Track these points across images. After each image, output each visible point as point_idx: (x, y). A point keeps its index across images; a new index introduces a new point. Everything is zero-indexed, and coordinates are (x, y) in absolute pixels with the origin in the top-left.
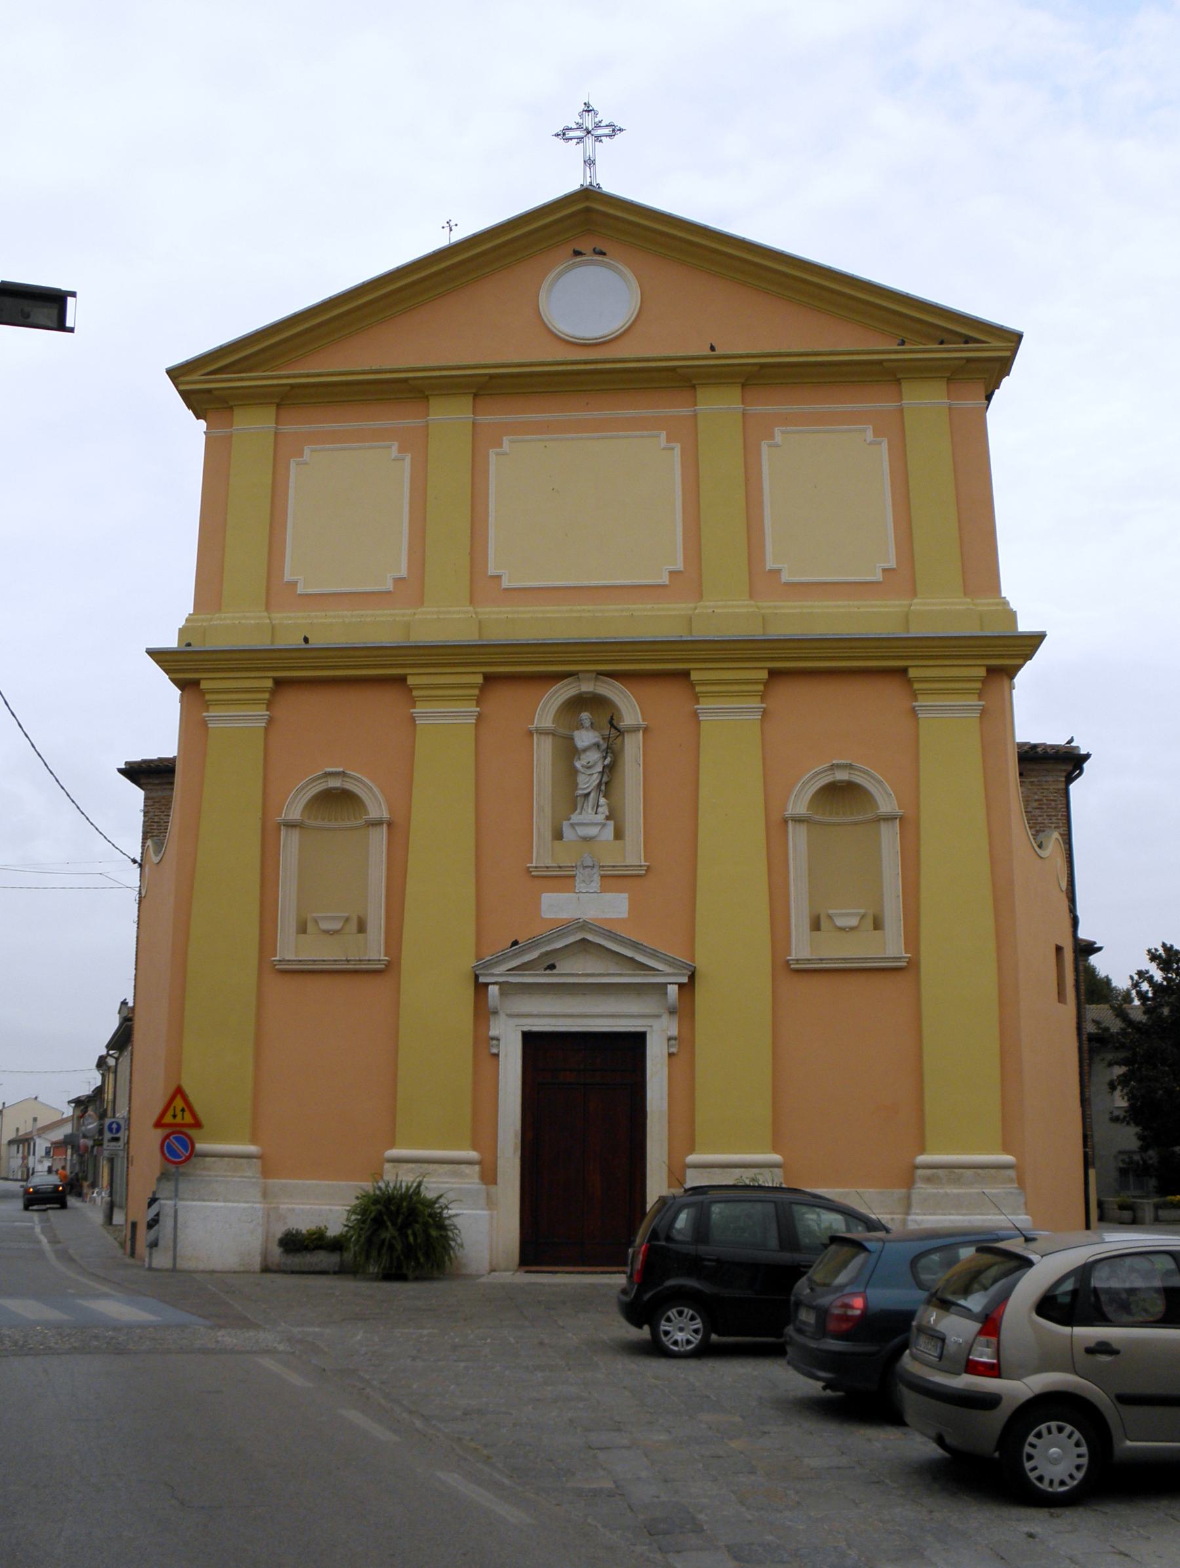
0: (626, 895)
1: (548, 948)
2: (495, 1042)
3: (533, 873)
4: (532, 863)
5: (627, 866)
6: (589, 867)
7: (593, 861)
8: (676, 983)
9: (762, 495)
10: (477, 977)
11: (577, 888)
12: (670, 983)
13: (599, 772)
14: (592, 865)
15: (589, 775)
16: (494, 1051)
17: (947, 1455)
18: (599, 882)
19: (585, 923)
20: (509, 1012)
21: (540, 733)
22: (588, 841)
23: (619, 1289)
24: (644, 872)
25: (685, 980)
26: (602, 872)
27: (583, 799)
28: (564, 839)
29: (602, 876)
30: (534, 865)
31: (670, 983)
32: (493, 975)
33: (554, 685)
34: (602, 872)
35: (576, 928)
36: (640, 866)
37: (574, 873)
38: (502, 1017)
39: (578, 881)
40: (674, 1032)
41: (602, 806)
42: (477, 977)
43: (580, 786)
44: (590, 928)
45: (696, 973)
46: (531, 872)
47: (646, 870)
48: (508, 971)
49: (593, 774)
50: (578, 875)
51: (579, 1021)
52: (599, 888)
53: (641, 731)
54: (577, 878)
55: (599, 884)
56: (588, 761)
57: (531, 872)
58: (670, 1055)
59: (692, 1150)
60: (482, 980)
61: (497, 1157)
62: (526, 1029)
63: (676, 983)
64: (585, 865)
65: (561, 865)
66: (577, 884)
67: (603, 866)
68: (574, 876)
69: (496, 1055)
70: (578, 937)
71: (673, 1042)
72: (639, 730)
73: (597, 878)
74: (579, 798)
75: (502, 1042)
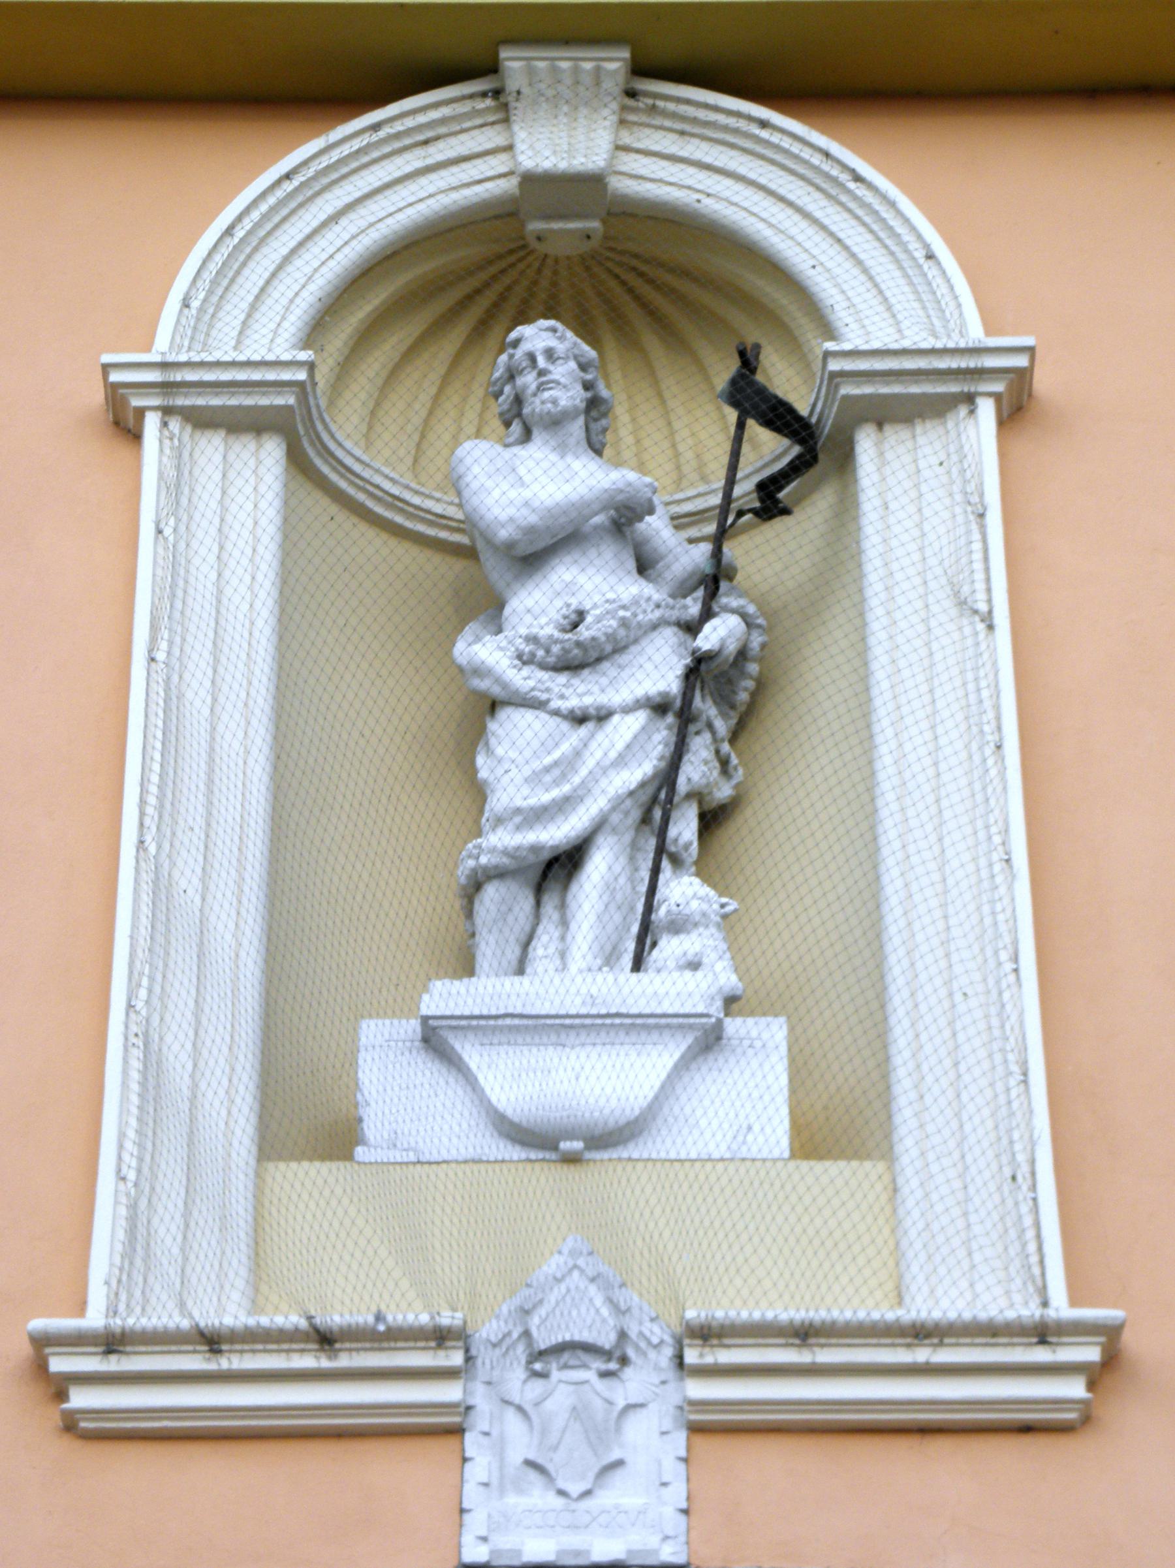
3: (80, 1399)
4: (81, 1308)
5: (920, 1333)
7: (619, 1311)
11: (475, 1524)
13: (660, 707)
14: (607, 1339)
15: (579, 719)
17: (702, 588)
18: (674, 1472)
21: (201, 420)
22: (572, 1159)
24: (1075, 1389)
26: (698, 1389)
27: (525, 902)
28: (360, 1152)
30: (95, 1318)
33: (318, 134)
34: (698, 1389)
36: (1043, 1333)
37: (450, 1392)
39: (479, 1469)
41: (678, 926)
43: (499, 801)
46: (60, 1387)
47: (1095, 1375)
49: (602, 716)
50: (481, 1421)
52: (677, 1524)
53: (986, 410)
54: (468, 1437)
55: (677, 1494)
56: (607, 1382)
57: (60, 1387)
64: (544, 1340)
65: (335, 1319)
66: (472, 1495)
67: (706, 1334)
72: (970, 399)
74: (492, 893)
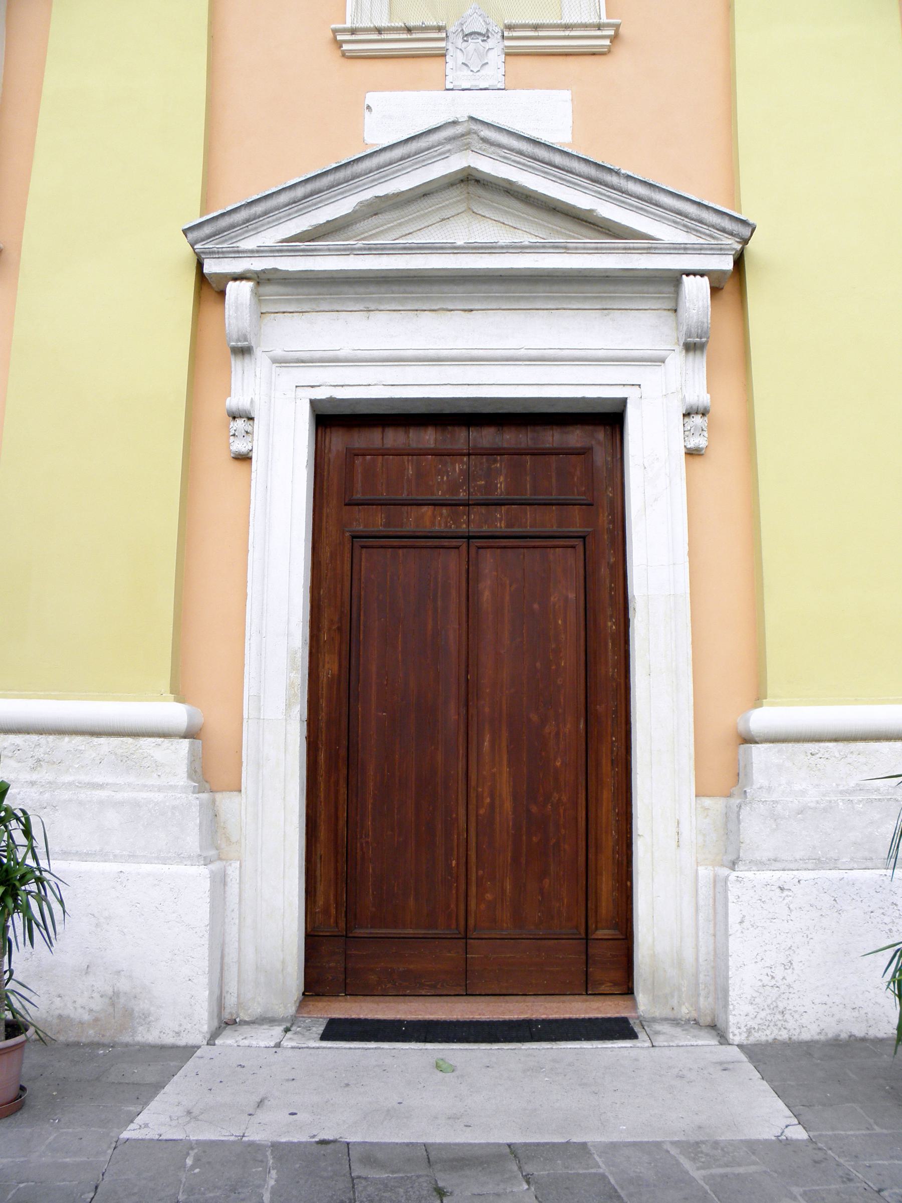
0: (566, 94)
1: (382, 190)
2: (240, 424)
3: (345, 47)
4: (345, 23)
5: (567, 27)
6: (479, 34)
8: (702, 274)
9: (439, 1042)
10: (200, 265)
12: (694, 273)
14: (484, 31)
16: (240, 446)
19: (474, 127)
20: (278, 352)
23: (253, 344)
25: (727, 264)
29: (510, 54)
31: (694, 273)
32: (238, 253)
35: (450, 140)
36: (599, 27)
38: (261, 361)
40: (699, 395)
42: (200, 265)
44: (485, 140)
45: (746, 258)
48: (283, 241)
50: (450, 53)
51: (472, 373)
55: (502, 71)
58: (692, 453)
59: (758, 698)
60: (211, 267)
61: (728, 967)
62: (322, 394)
63: (702, 274)
65: (412, 23)
66: (448, 72)
68: (442, 55)
69: (244, 458)
70: (455, 163)
71: (697, 420)
73: (496, 58)
75: (259, 426)
